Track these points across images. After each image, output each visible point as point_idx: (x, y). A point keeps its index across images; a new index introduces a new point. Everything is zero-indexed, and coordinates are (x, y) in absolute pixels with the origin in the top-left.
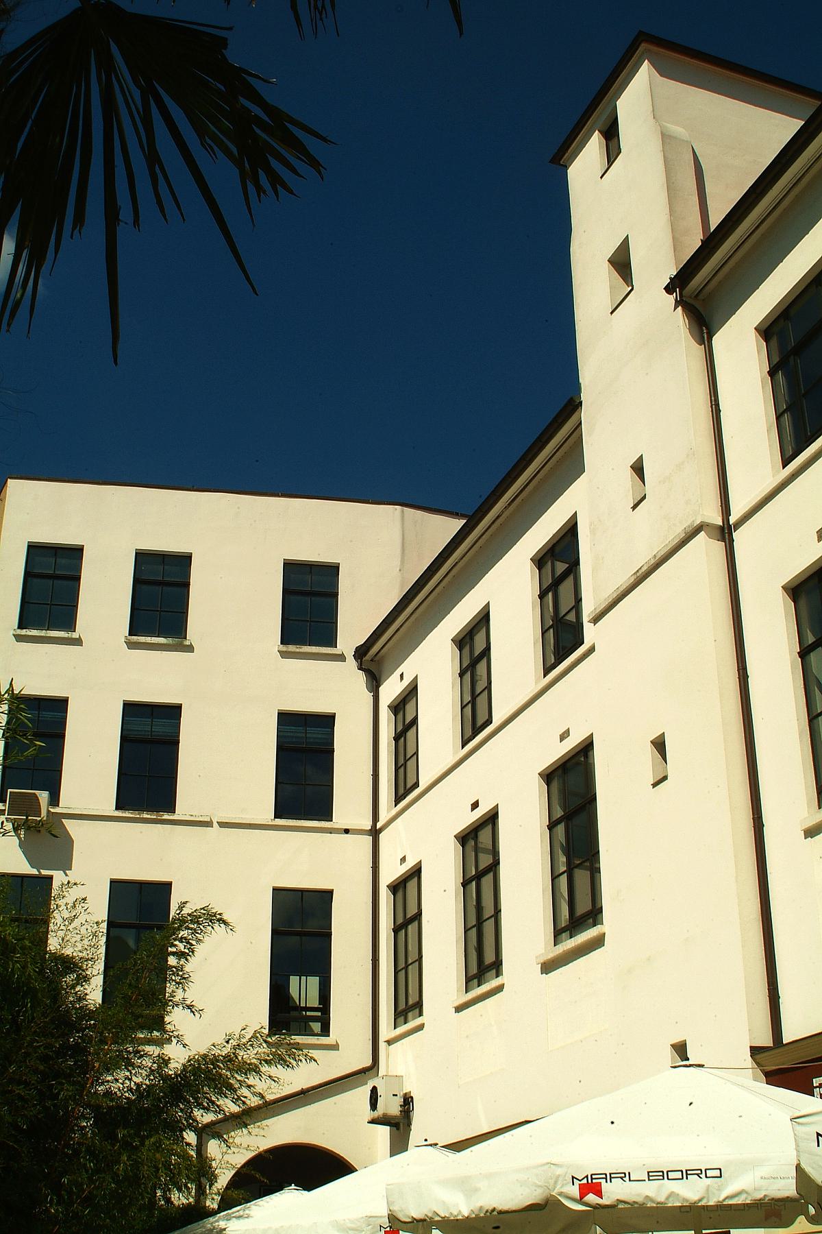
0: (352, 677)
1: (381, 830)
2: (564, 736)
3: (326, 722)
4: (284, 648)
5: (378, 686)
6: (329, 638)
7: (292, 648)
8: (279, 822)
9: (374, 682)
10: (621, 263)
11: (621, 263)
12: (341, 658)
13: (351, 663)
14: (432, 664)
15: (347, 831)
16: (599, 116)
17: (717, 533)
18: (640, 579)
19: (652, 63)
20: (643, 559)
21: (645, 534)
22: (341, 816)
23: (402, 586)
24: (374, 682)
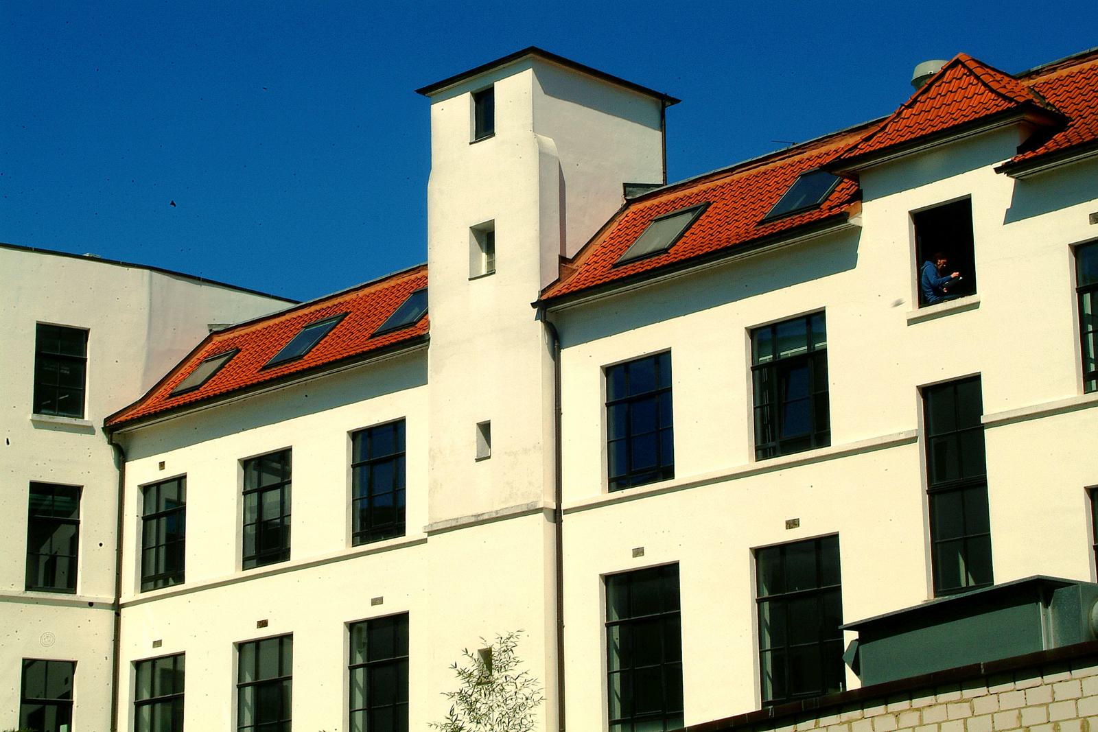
0: (102, 450)
1: (123, 606)
2: (377, 601)
3: (74, 493)
4: (37, 417)
5: (125, 461)
6: (74, 406)
7: (45, 418)
8: (31, 594)
9: (122, 456)
10: (485, 236)
11: (485, 236)
12: (89, 430)
13: (100, 438)
14: (211, 473)
15: (91, 604)
16: (479, 83)
17: (551, 515)
18: (479, 522)
19: (534, 70)
20: (486, 507)
21: (486, 488)
22: (84, 590)
23: (152, 356)
24: (122, 456)
